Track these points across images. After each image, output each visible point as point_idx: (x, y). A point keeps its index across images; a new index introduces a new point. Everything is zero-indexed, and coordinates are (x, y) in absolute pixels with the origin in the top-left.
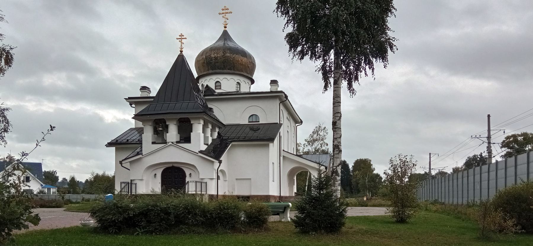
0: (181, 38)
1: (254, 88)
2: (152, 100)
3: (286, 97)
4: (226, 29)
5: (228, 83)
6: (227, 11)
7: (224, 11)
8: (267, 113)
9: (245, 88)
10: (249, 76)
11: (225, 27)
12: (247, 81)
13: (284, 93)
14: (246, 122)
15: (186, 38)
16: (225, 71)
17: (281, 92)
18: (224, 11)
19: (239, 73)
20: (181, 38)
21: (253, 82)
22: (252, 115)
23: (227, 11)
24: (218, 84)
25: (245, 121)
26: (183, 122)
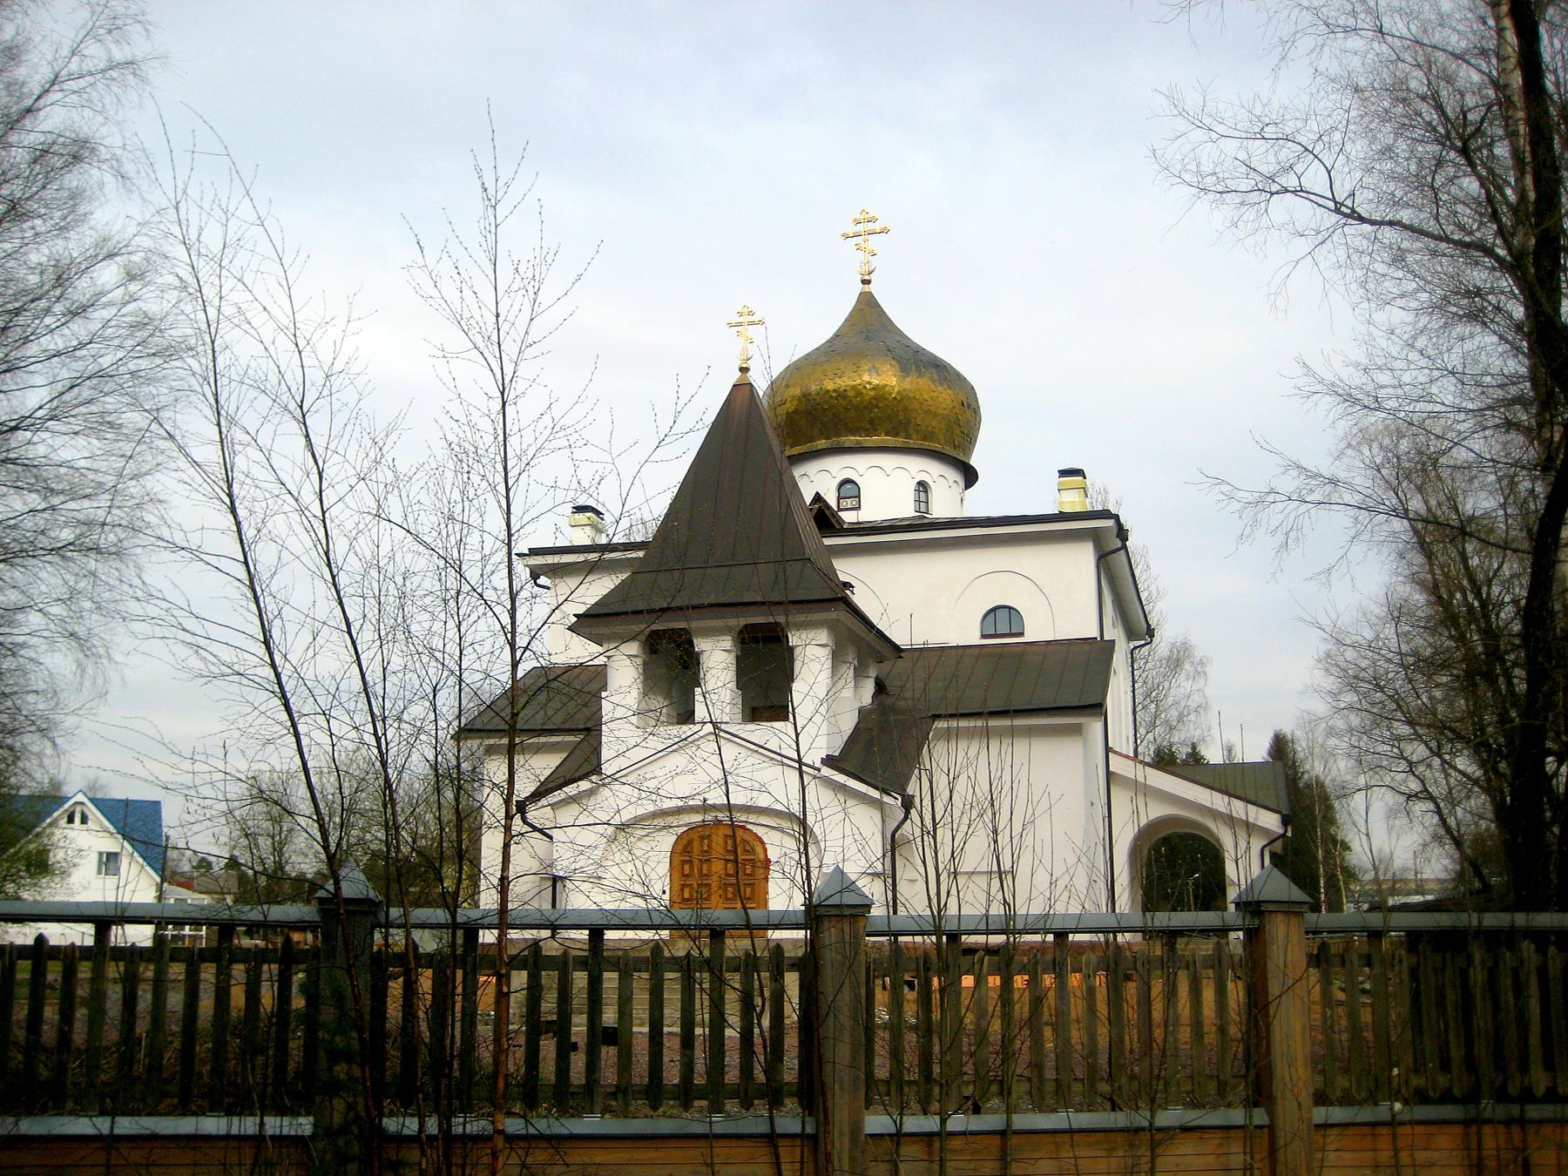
0: (866, 229)
1: (981, 502)
2: (641, 554)
3: (1122, 534)
4: (872, 288)
5: (885, 485)
6: (870, 226)
7: (860, 228)
8: (1057, 599)
9: (947, 500)
10: (961, 457)
11: (866, 282)
12: (953, 476)
13: (1116, 518)
14: (972, 637)
15: (884, 231)
16: (849, 440)
17: (1105, 514)
18: (860, 228)
19: (926, 445)
20: (866, 229)
21: (970, 477)
22: (994, 610)
23: (870, 226)
24: (849, 488)
25: (967, 633)
26: (756, 640)
